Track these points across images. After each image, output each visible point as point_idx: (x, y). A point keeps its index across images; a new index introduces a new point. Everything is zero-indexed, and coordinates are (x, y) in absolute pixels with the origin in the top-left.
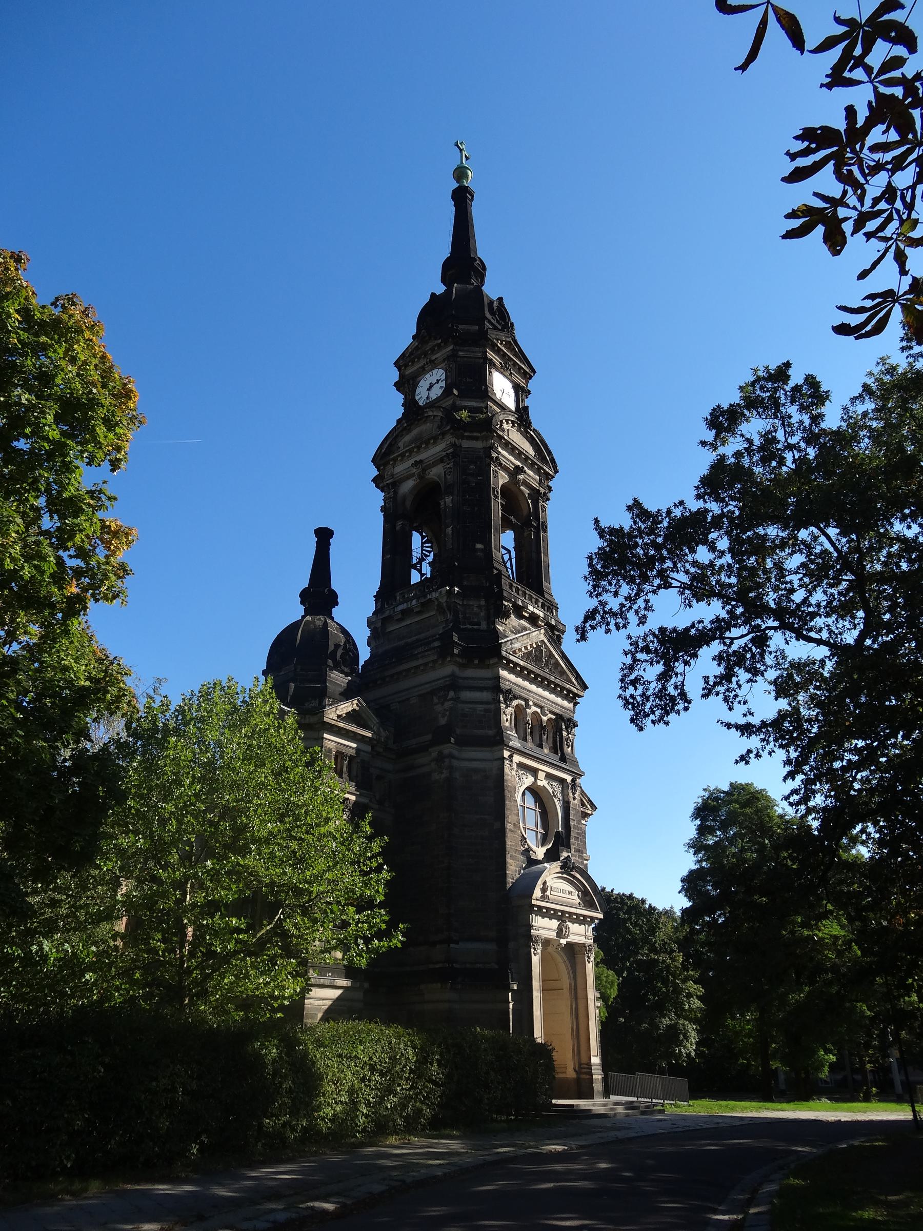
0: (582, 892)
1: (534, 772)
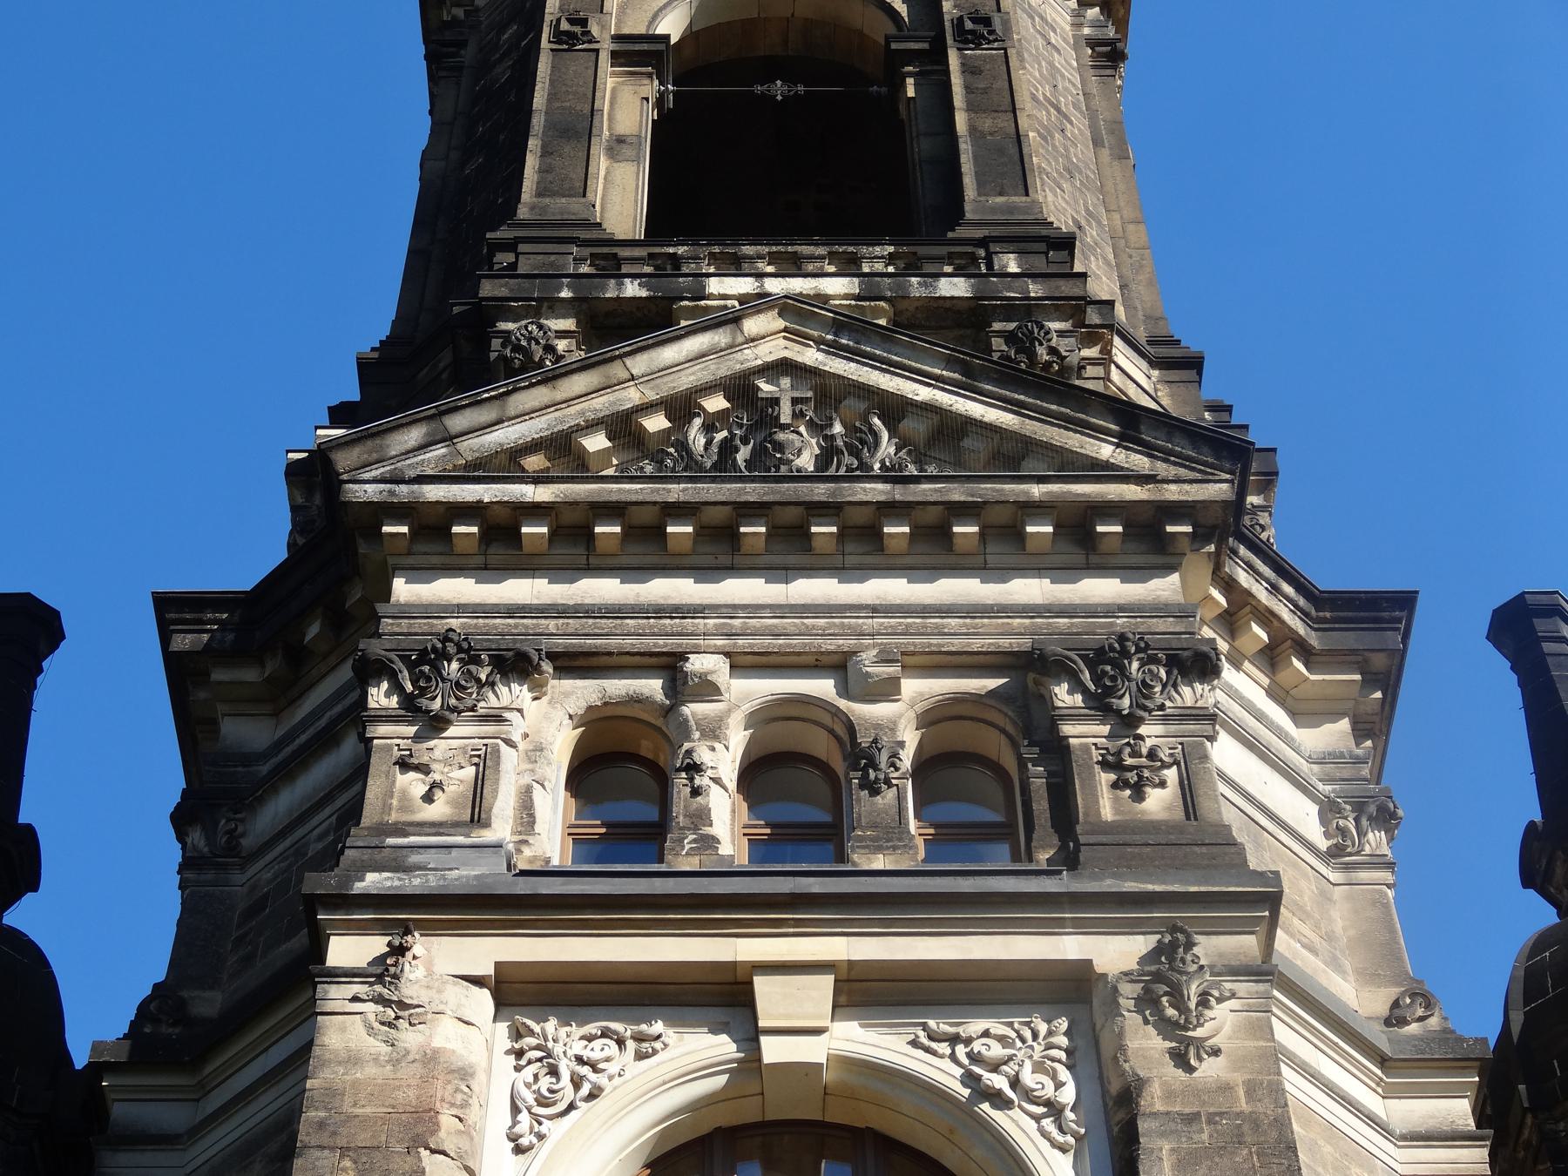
1: (725, 998)
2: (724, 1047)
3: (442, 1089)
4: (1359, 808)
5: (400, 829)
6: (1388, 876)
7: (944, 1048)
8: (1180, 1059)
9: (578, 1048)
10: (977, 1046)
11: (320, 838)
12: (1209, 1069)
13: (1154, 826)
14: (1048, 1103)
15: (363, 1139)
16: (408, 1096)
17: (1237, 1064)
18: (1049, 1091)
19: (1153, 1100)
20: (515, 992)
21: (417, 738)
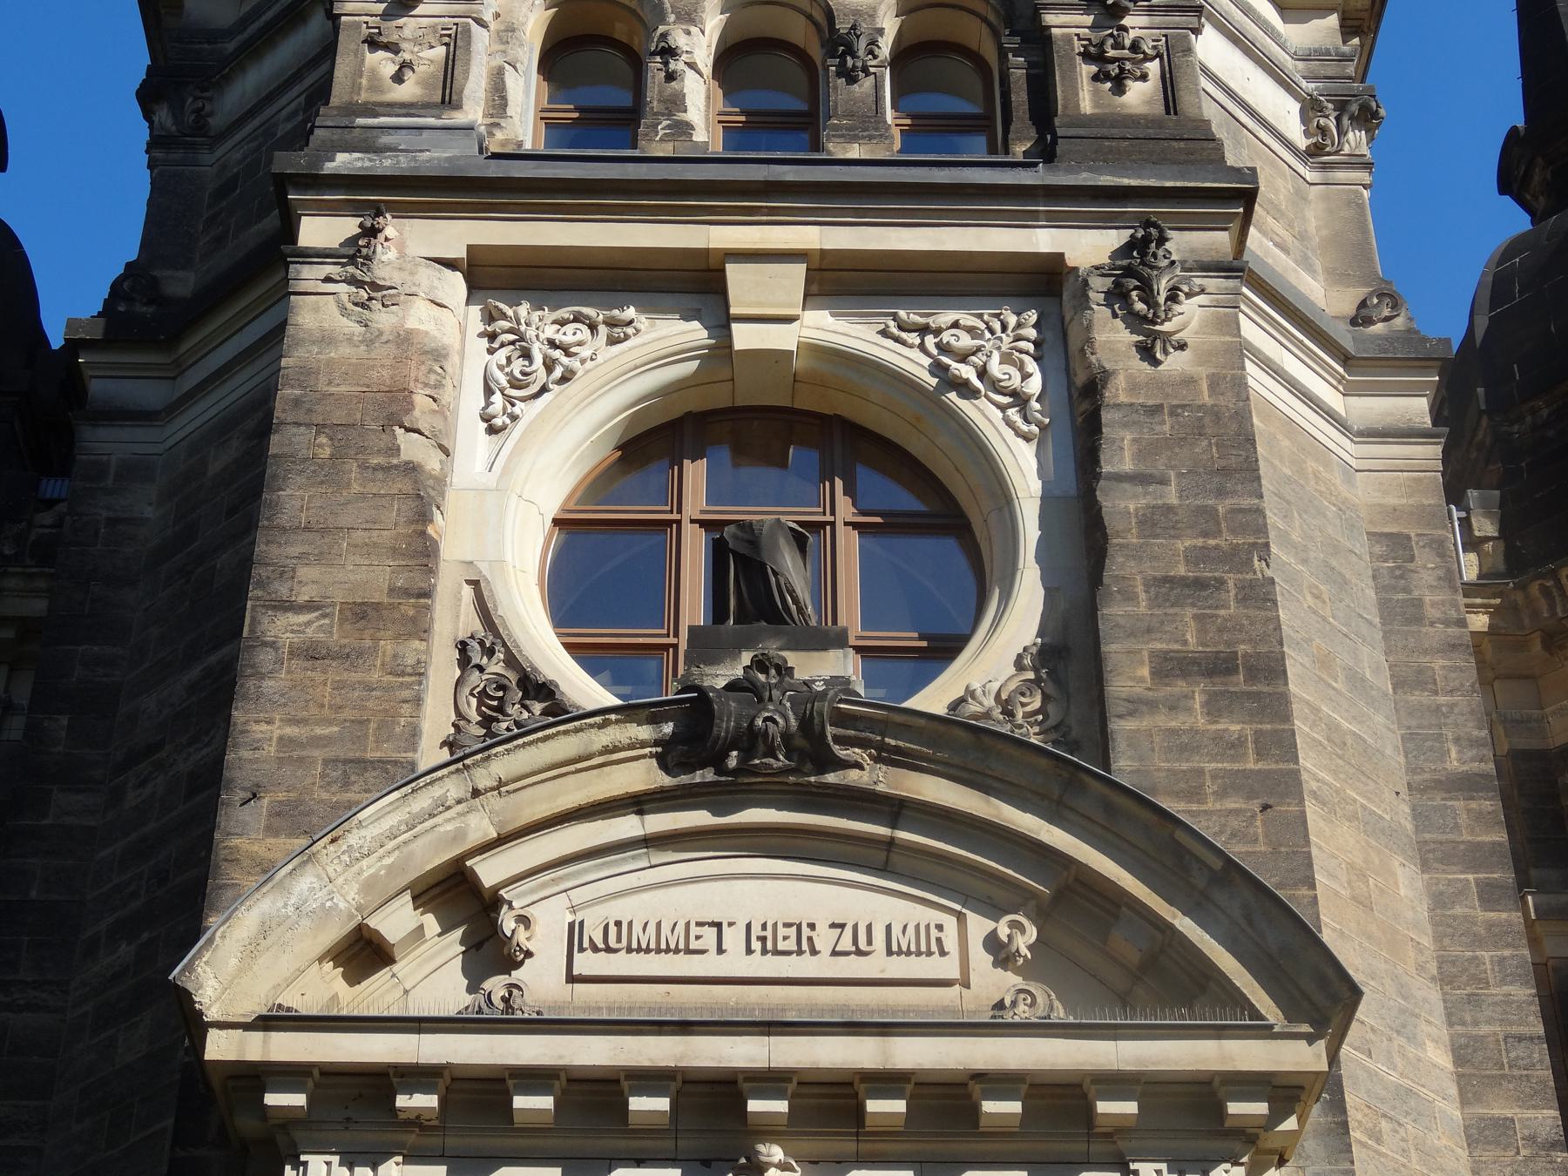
0: (1041, 916)
1: (697, 285)
2: (694, 333)
3: (415, 370)
4: (1341, 107)
5: (371, 110)
6: (1364, 176)
7: (913, 338)
8: (1146, 352)
9: (550, 331)
10: (946, 337)
11: (289, 118)
12: (1174, 363)
13: (1132, 120)
14: (1014, 394)
15: (338, 416)
17: (1204, 357)
18: (1016, 381)
19: (1117, 392)
20: (488, 276)
21: (386, 16)
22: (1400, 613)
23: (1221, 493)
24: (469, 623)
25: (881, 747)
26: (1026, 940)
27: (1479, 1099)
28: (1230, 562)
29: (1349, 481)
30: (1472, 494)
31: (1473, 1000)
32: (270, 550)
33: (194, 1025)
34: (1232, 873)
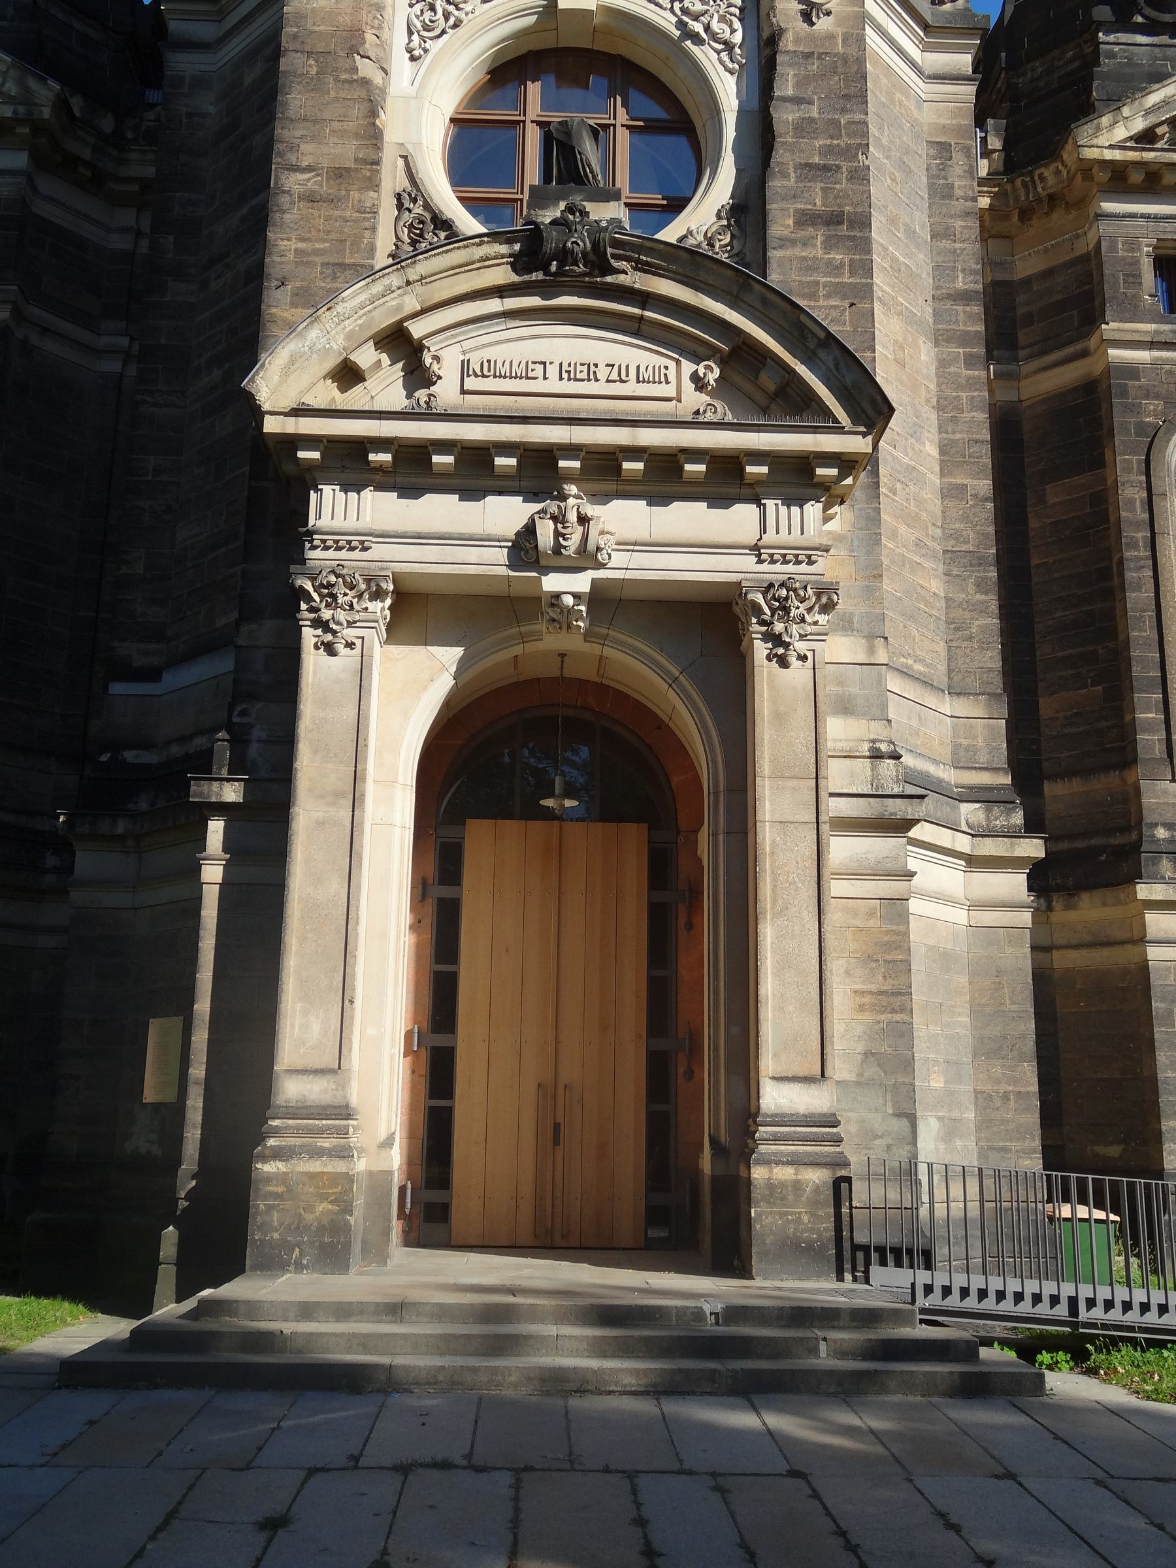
0: (724, 362)
3: (366, 17)
8: (807, 17)
12: (823, 24)
14: (726, 43)
15: (320, 47)
16: (345, 20)
17: (839, 23)
18: (727, 35)
19: (788, 43)
22: (940, 192)
23: (843, 110)
24: (403, 183)
25: (638, 261)
26: (713, 376)
27: (950, 474)
28: (846, 158)
29: (919, 108)
30: (990, 121)
31: (954, 420)
32: (285, 133)
33: (256, 413)
34: (830, 340)
